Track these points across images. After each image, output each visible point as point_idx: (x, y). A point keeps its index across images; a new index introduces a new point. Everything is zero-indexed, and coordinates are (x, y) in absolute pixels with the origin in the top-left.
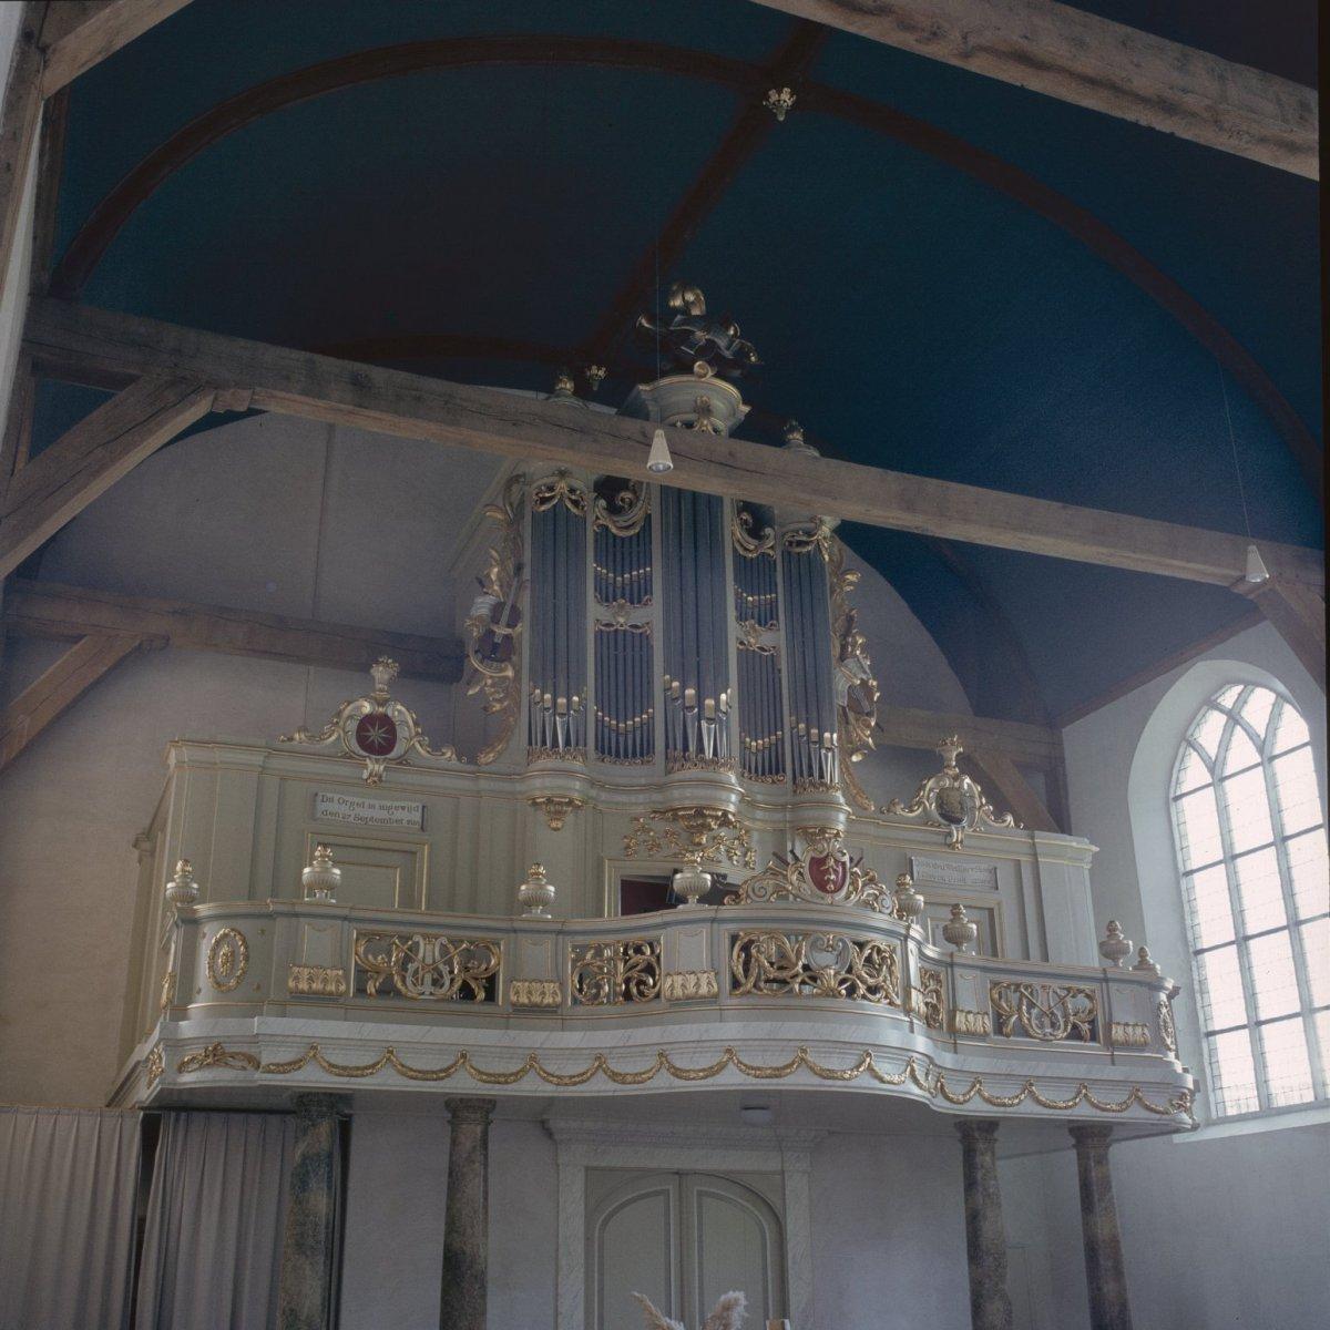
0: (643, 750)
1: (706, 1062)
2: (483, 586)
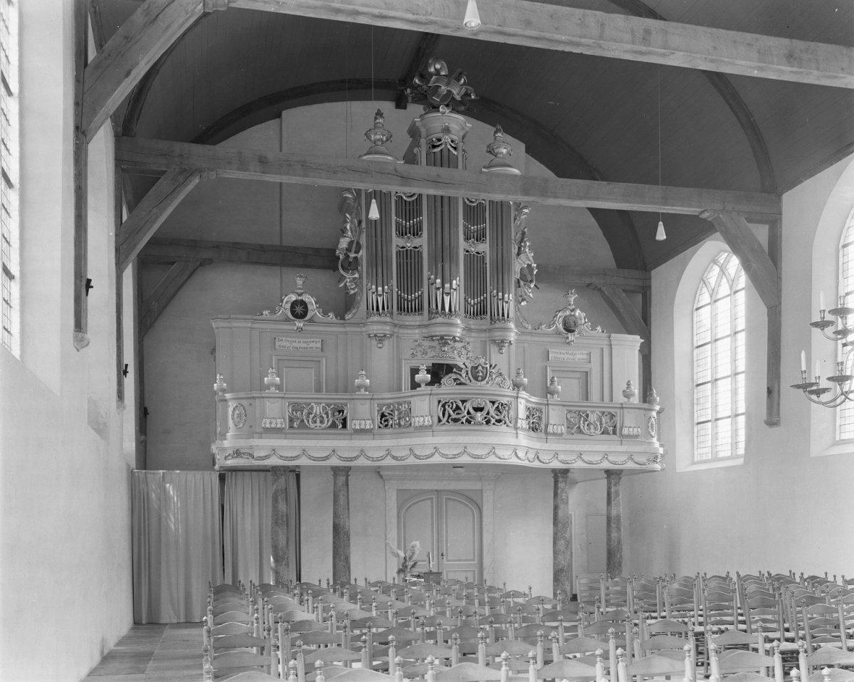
0: (419, 309)
1: (428, 452)
2: (344, 233)
